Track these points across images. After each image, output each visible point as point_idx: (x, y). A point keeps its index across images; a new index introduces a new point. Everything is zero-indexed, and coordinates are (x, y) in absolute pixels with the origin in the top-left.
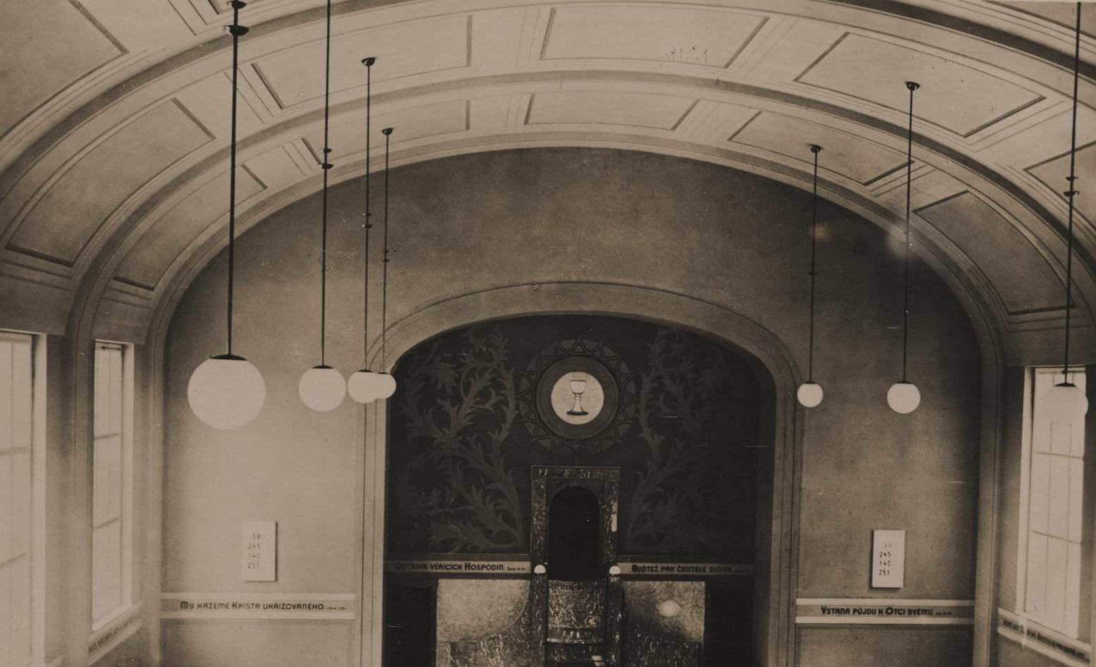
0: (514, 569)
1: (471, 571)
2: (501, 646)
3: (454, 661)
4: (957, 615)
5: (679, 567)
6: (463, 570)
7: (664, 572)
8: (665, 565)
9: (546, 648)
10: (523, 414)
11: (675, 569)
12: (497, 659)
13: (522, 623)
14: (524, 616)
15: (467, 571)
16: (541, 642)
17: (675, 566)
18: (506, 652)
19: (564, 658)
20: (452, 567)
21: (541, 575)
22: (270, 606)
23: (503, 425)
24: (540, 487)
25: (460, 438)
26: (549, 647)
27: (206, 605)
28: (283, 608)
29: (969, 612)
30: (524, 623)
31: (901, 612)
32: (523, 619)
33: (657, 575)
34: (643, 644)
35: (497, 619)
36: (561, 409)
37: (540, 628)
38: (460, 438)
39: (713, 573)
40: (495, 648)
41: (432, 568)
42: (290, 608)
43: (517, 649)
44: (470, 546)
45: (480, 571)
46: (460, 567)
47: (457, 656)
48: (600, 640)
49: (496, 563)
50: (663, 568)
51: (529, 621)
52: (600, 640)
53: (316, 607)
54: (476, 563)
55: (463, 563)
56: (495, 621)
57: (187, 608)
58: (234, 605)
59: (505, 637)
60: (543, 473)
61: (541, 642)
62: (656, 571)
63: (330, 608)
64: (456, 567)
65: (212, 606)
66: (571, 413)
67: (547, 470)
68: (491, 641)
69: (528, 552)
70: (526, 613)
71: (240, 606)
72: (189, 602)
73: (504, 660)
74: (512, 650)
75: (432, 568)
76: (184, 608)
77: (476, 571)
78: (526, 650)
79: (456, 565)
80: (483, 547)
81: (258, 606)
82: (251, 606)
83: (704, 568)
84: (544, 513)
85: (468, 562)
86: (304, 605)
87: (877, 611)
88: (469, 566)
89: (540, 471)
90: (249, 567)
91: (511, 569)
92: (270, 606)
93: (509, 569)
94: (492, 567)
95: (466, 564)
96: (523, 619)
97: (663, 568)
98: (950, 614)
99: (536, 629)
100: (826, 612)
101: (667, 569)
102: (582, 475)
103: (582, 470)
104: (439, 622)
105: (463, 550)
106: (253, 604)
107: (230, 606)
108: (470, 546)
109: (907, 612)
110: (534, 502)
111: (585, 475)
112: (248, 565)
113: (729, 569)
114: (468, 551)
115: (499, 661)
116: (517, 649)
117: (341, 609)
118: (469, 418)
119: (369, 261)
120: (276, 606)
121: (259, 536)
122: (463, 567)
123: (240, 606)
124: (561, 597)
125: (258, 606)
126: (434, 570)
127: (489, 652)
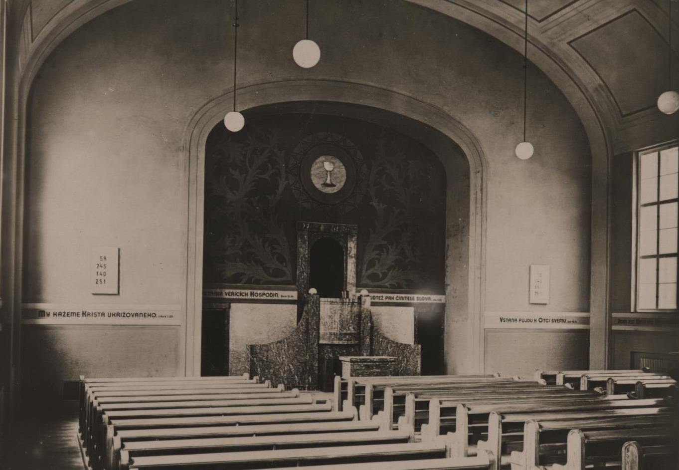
0: (286, 296)
1: (255, 297)
2: (286, 348)
3: (252, 359)
4: (580, 323)
5: (398, 297)
6: (249, 297)
7: (387, 300)
8: (388, 295)
9: (319, 348)
10: (291, 183)
11: (395, 298)
12: (283, 358)
13: (301, 331)
14: (302, 325)
15: (252, 298)
16: (315, 344)
17: (395, 295)
18: (289, 352)
19: (331, 356)
20: (241, 294)
21: (314, 294)
22: (114, 315)
23: (277, 191)
24: (304, 237)
25: (246, 199)
26: (321, 346)
27: (60, 314)
28: (124, 316)
29: (586, 321)
30: (302, 331)
31: (547, 321)
32: (301, 327)
33: (383, 302)
34: (384, 346)
35: (274, 334)
36: (317, 183)
37: (314, 334)
38: (246, 199)
39: (419, 301)
40: (281, 349)
41: (226, 295)
42: (130, 316)
43: (297, 350)
44: (253, 279)
45: (262, 298)
46: (247, 294)
47: (254, 355)
48: (356, 342)
49: (273, 292)
50: (386, 298)
51: (305, 329)
52: (356, 342)
53: (150, 315)
54: (259, 292)
55: (249, 292)
56: (272, 335)
57: (44, 316)
58: (84, 314)
59: (288, 341)
60: (306, 227)
61: (315, 344)
62: (382, 299)
63: (161, 316)
64: (243, 294)
65: (66, 315)
66: (325, 185)
67: (309, 224)
68: (278, 344)
69: (295, 285)
70: (304, 324)
71: (89, 314)
72: (46, 311)
73: (288, 358)
74: (294, 351)
75: (226, 295)
76: (42, 316)
77: (258, 297)
78: (304, 351)
79: (244, 293)
80: (265, 277)
81: (103, 314)
82: (97, 314)
83: (413, 298)
84: (307, 256)
85: (252, 291)
86: (140, 314)
87: (533, 320)
88: (253, 294)
89: (304, 226)
90: (97, 283)
91: (283, 296)
92: (114, 315)
93: (282, 296)
94: (270, 295)
95: (251, 292)
96: (301, 327)
97: (386, 298)
98: (576, 322)
99: (312, 335)
100: (503, 321)
101: (390, 298)
102: (333, 229)
103: (333, 226)
104: (231, 335)
105: (249, 282)
106: (99, 313)
107: (81, 315)
108: (253, 279)
109: (551, 321)
110: (300, 247)
111: (335, 229)
112: (96, 281)
113: (429, 299)
114: (253, 283)
115: (284, 359)
116: (297, 350)
117: (170, 317)
118: (253, 184)
119: (237, 57)
120: (118, 314)
121: (105, 258)
122: (249, 295)
123: (89, 314)
124: (130, 467)
125: (103, 314)
126: (228, 297)
127: (277, 352)
